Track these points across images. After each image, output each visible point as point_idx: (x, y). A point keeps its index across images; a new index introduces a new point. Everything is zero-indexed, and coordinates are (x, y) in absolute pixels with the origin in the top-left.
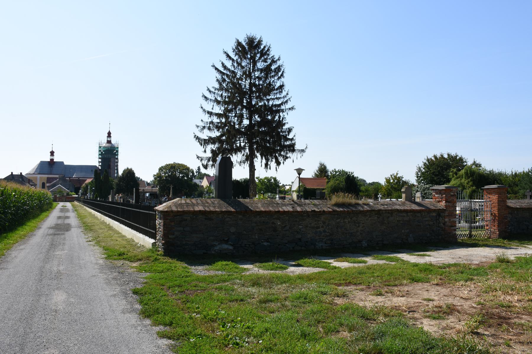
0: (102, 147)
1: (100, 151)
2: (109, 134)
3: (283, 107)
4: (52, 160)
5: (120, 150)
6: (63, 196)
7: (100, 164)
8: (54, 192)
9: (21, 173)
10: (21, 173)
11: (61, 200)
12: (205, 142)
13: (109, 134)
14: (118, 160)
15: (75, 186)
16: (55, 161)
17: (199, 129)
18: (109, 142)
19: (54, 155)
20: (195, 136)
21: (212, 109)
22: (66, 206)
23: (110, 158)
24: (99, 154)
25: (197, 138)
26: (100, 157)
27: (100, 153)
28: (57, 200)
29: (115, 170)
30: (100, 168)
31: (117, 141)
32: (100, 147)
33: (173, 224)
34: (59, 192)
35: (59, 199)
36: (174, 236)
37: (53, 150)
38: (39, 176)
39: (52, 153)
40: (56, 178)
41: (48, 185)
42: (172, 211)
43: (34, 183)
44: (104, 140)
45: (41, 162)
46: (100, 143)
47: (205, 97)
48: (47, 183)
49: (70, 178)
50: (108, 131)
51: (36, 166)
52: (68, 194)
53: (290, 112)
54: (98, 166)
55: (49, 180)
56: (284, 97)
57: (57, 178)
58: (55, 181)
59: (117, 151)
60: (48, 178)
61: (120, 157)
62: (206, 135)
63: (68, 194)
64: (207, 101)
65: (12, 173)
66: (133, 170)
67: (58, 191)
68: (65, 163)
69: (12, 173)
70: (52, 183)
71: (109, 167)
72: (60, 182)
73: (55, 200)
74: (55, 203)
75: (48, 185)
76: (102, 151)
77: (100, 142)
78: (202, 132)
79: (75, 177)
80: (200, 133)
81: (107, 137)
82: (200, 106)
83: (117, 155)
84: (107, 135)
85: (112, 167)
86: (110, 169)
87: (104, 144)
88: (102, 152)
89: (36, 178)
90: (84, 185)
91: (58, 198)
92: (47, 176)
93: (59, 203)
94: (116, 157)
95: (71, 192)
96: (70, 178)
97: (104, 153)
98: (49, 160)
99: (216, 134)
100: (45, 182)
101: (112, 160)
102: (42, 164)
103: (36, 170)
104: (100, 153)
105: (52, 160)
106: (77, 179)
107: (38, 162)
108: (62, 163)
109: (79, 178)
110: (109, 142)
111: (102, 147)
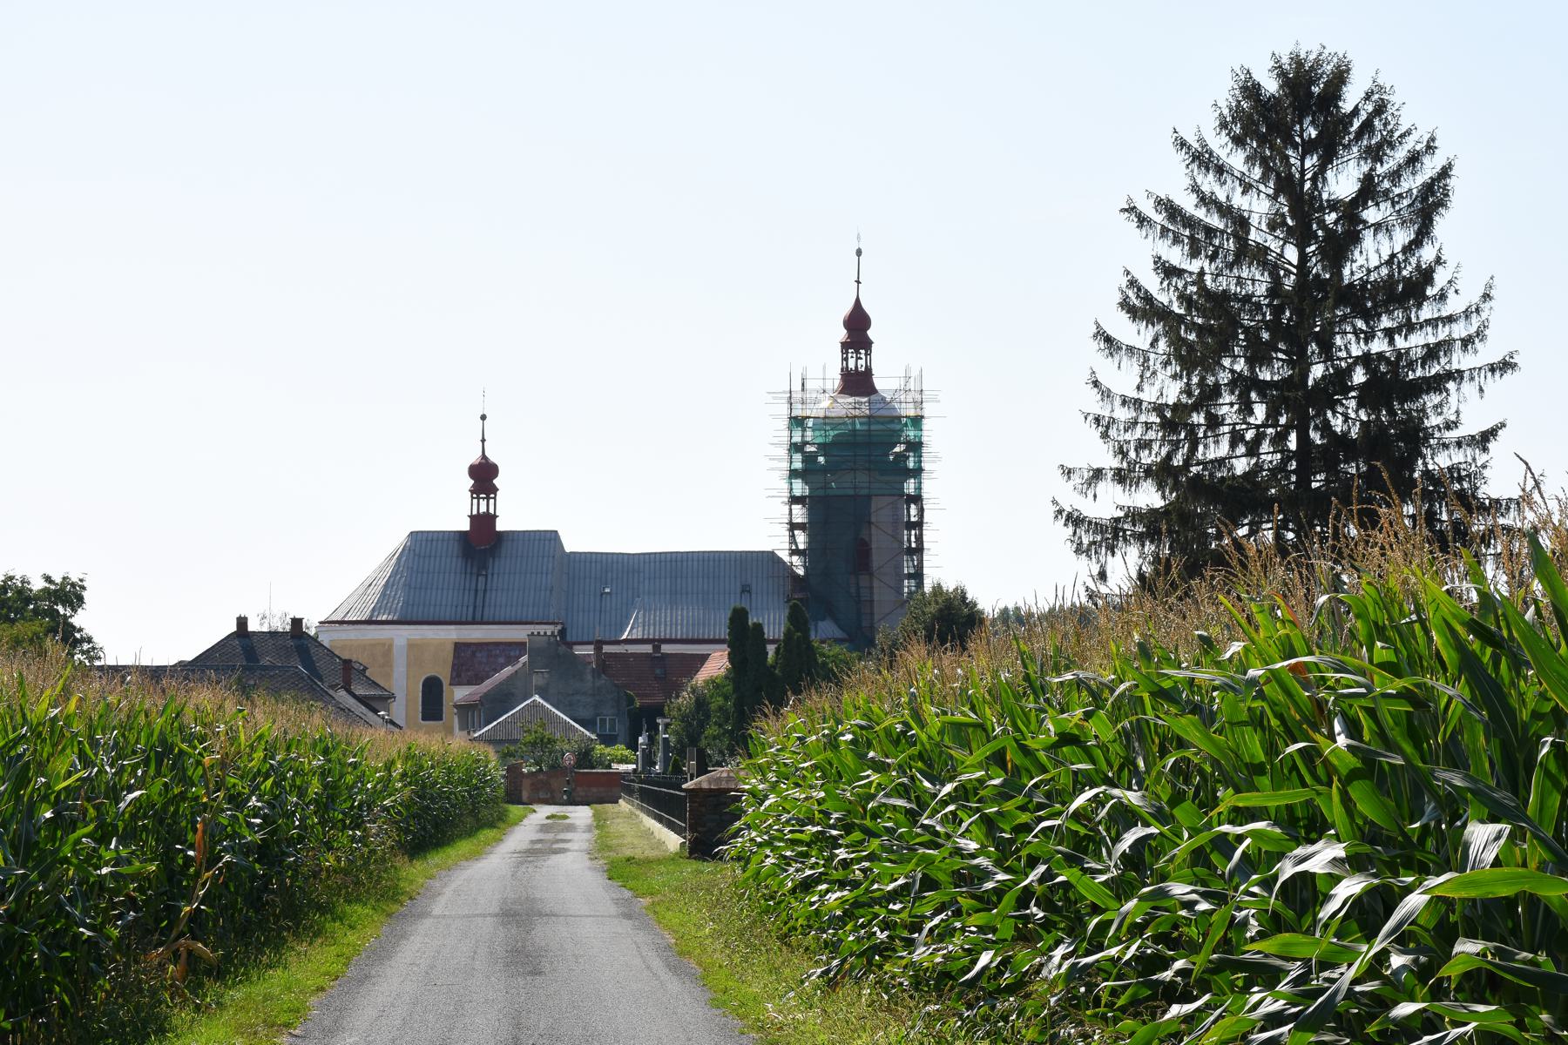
0: (810, 423)
1: (795, 448)
2: (857, 327)
3: (1460, 360)
4: (483, 522)
5: (931, 434)
6: (555, 767)
7: (801, 539)
8: (501, 742)
9: (297, 623)
10: (297, 623)
11: (542, 795)
12: (1110, 535)
13: (857, 327)
14: (921, 511)
15: (631, 701)
16: (501, 526)
17: (1076, 480)
18: (857, 382)
19: (495, 490)
20: (1060, 512)
21: (1139, 388)
22: (566, 817)
23: (869, 497)
24: (793, 474)
25: (1075, 520)
26: (799, 488)
27: (798, 465)
28: (525, 795)
29: (901, 577)
30: (798, 566)
31: (914, 373)
32: (797, 422)
33: (703, 809)
34: (534, 744)
35: (535, 788)
36: (705, 829)
37: (493, 457)
38: (402, 635)
39: (484, 476)
40: (509, 650)
41: (461, 693)
42: (701, 789)
43: (375, 685)
44: (828, 366)
45: (414, 535)
46: (797, 396)
47: (1108, 340)
48: (458, 679)
49: (599, 645)
50: (848, 307)
51: (381, 569)
52: (585, 757)
53: (1494, 384)
54: (784, 555)
55: (469, 661)
56: (1467, 314)
57: (520, 647)
58: (508, 671)
59: (916, 447)
60: (459, 647)
61: (931, 488)
62: (1108, 502)
63: (585, 757)
64: (1117, 358)
65: (242, 622)
66: (969, 596)
67: (530, 738)
68: (572, 543)
69: (242, 622)
70: (488, 685)
71: (861, 558)
72: (537, 680)
73: (514, 797)
74: (515, 810)
75: (461, 693)
76: (809, 449)
77: (797, 387)
78: (1090, 494)
79: (638, 634)
80: (1082, 498)
81: (845, 346)
82: (1087, 375)
83: (918, 472)
84: (842, 334)
85: (877, 559)
86: (871, 575)
87: (826, 399)
88: (809, 459)
89: (387, 649)
90: (685, 699)
91: (526, 783)
92: (452, 634)
93: (535, 807)
94: (910, 487)
95: (608, 740)
96: (599, 645)
97: (821, 459)
98: (465, 526)
99: (1149, 497)
100: (444, 675)
101: (880, 510)
102: (422, 546)
103: (383, 594)
104: (798, 465)
105: (483, 522)
106: (648, 649)
107: (394, 540)
108: (552, 537)
109: (657, 643)
110: (857, 382)
111: (810, 423)
